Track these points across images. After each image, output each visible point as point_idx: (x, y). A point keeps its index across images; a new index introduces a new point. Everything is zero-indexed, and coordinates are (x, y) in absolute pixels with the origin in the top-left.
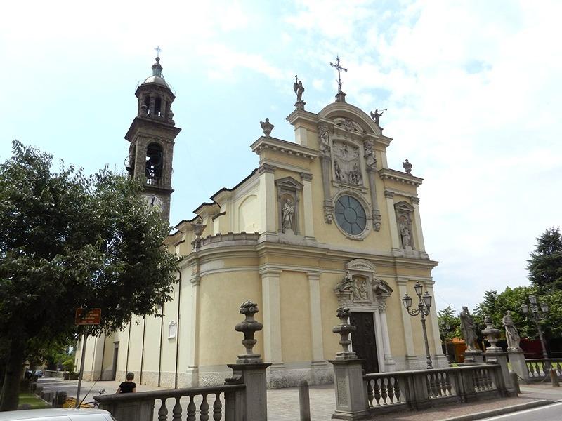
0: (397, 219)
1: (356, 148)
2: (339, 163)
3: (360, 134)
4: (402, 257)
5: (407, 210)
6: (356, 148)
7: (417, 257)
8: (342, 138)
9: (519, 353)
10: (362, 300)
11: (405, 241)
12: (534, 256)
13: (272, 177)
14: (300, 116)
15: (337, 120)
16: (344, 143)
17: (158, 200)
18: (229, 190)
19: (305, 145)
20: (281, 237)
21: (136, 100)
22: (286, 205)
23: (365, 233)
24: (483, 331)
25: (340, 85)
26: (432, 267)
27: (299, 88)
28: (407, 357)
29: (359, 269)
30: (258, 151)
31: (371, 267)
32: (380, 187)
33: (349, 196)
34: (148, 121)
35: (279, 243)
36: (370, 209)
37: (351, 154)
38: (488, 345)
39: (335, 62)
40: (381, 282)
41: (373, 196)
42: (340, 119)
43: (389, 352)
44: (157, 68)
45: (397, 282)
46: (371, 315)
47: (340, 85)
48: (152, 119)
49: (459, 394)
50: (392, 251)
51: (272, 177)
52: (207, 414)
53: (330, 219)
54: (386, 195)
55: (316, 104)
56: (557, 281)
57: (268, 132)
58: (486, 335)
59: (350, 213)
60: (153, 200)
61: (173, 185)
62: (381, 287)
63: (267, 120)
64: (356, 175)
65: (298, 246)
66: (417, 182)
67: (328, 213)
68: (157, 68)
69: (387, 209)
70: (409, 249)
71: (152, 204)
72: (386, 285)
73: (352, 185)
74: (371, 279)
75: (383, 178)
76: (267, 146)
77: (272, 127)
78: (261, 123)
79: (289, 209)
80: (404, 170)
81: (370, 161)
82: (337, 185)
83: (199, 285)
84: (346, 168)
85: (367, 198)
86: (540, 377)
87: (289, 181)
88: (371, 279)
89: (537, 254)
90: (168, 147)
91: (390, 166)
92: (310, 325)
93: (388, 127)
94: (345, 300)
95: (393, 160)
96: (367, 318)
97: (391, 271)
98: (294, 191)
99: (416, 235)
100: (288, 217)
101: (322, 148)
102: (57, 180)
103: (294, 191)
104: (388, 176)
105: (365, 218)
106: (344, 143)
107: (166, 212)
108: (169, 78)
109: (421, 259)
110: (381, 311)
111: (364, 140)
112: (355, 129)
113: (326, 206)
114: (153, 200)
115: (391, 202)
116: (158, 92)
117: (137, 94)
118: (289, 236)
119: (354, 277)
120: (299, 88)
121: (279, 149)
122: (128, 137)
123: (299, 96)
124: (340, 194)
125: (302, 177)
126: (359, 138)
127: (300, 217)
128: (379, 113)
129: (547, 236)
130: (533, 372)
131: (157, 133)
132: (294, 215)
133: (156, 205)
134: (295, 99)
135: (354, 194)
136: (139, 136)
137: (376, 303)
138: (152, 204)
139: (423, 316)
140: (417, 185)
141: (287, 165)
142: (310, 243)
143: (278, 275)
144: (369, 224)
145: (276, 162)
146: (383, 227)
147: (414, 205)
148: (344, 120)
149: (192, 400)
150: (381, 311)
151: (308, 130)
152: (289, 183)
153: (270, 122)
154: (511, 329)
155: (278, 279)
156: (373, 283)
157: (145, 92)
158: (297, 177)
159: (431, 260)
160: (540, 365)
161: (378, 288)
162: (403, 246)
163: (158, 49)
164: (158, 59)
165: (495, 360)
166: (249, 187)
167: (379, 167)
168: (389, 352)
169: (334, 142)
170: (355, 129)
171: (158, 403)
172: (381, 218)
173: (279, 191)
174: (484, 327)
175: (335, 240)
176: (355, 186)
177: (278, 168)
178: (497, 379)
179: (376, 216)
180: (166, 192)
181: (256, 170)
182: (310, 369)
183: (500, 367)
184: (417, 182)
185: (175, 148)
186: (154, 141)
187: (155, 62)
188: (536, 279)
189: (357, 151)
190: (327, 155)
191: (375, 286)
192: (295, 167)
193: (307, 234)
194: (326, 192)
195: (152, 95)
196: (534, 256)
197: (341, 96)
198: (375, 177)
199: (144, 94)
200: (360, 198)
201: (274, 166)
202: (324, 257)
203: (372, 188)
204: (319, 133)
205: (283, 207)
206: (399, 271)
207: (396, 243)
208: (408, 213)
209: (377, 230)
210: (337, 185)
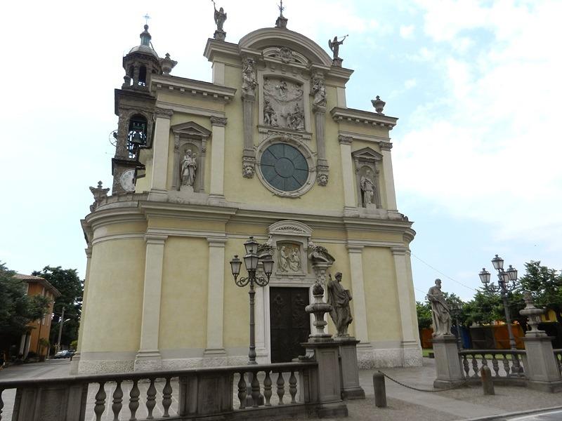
1: (299, 84)
2: (273, 104)
3: (304, 64)
7: (383, 217)
8: (278, 73)
9: (446, 341)
10: (291, 272)
11: (367, 197)
14: (217, 48)
15: (267, 52)
16: (282, 79)
19: (222, 83)
20: (174, 196)
23: (305, 188)
27: (220, 17)
28: (403, 342)
29: (286, 232)
31: (306, 231)
32: (332, 131)
33: (284, 143)
34: (131, 93)
35: (167, 202)
36: (314, 158)
37: (292, 92)
40: (319, 250)
41: (320, 143)
44: (146, 36)
45: (348, 249)
47: (281, 9)
48: (135, 90)
52: (103, 404)
53: (249, 171)
54: (340, 141)
59: (284, 164)
62: (316, 255)
63: (378, 97)
64: (298, 116)
65: (200, 206)
66: (389, 123)
68: (146, 36)
69: (340, 159)
70: (371, 207)
72: (324, 252)
73: (287, 130)
74: (305, 246)
75: (336, 119)
77: (383, 104)
78: (372, 101)
79: (188, 160)
80: (373, 110)
81: (318, 99)
82: (266, 130)
83: (91, 258)
84: (281, 110)
85: (311, 146)
86: (498, 376)
87: (368, 152)
88: (305, 246)
91: (349, 105)
92: (206, 303)
94: (322, 274)
95: (356, 97)
96: (299, 295)
98: (373, 162)
99: (385, 190)
100: (186, 171)
101: (245, 85)
103: (373, 162)
106: (282, 79)
111: (309, 73)
112: (297, 61)
113: (247, 157)
115: (347, 150)
116: (141, 61)
118: (187, 194)
119: (280, 244)
120: (220, 17)
121: (354, 119)
124: (270, 141)
125: (381, 147)
126: (302, 72)
127: (206, 171)
128: (339, 40)
130: (467, 370)
131: (140, 104)
132: (197, 169)
134: (215, 28)
135: (291, 141)
139: (252, 287)
141: (191, 108)
142: (214, 202)
143: (360, 251)
144: (312, 177)
145: (173, 105)
147: (384, 153)
148: (279, 50)
149: (119, 387)
152: (367, 154)
153: (172, 58)
154: (438, 306)
155: (360, 255)
156: (309, 250)
158: (204, 123)
160: (509, 357)
163: (147, 17)
164: (146, 27)
167: (332, 104)
169: (266, 78)
170: (297, 61)
171: (93, 390)
172: (329, 169)
173: (357, 163)
175: (257, 196)
176: (292, 131)
177: (174, 112)
178: (307, 386)
179: (322, 168)
182: (201, 358)
183: (316, 366)
184: (389, 123)
186: (137, 113)
189: (301, 88)
190: (251, 93)
193: (213, 191)
194: (248, 139)
195: (136, 64)
197: (282, 21)
200: (300, 146)
201: (169, 110)
202: (233, 218)
205: (181, 159)
207: (352, 198)
209: (323, 184)
210: (266, 130)
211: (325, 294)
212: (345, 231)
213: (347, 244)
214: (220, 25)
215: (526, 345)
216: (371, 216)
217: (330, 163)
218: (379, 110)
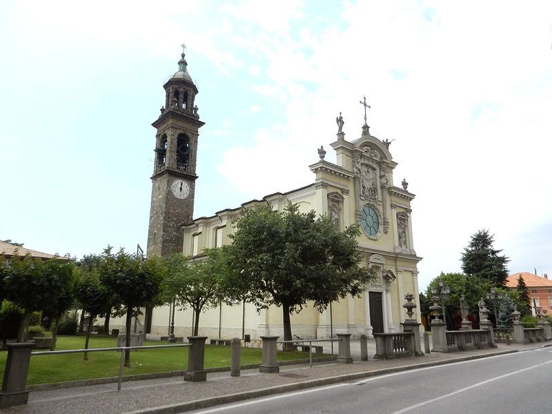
0: (398, 225)
1: (374, 169)
4: (400, 254)
5: (404, 218)
6: (374, 169)
7: (409, 253)
8: (366, 162)
10: (377, 284)
12: (467, 250)
13: (326, 192)
14: (342, 145)
16: (367, 165)
17: (186, 185)
18: (281, 194)
19: (345, 167)
21: (164, 93)
22: (333, 213)
23: (379, 234)
24: (430, 307)
25: (365, 119)
26: (418, 261)
27: (340, 121)
30: (316, 171)
31: (383, 260)
36: (382, 217)
37: (371, 175)
38: (434, 317)
39: (363, 101)
40: (389, 271)
41: (384, 207)
42: (367, 148)
43: (391, 321)
44: (183, 63)
46: (380, 294)
47: (365, 119)
49: (475, 345)
50: (394, 249)
51: (326, 192)
54: (392, 206)
55: (353, 135)
56: (483, 272)
57: (322, 157)
58: (432, 310)
61: (198, 172)
64: (374, 190)
66: (410, 197)
67: (358, 219)
68: (183, 63)
69: (392, 215)
75: (391, 193)
76: (323, 168)
80: (401, 187)
81: (384, 181)
82: (363, 198)
84: (368, 185)
89: (470, 249)
93: (395, 152)
95: (396, 181)
97: (393, 263)
104: (392, 191)
105: (378, 224)
106: (367, 165)
108: (194, 74)
109: (411, 255)
110: (387, 291)
111: (379, 164)
115: (395, 212)
117: (166, 86)
120: (340, 121)
122: (155, 125)
123: (340, 128)
128: (388, 141)
129: (479, 236)
131: (186, 125)
135: (373, 205)
137: (384, 286)
140: (411, 199)
144: (381, 228)
145: (328, 180)
146: (389, 230)
147: (408, 215)
150: (387, 291)
151: (346, 155)
159: (417, 256)
161: (387, 276)
162: (400, 245)
163: (184, 46)
164: (183, 56)
165: (487, 327)
166: (307, 194)
168: (391, 321)
174: (432, 304)
177: (330, 185)
179: (386, 223)
180: (192, 178)
181: (313, 184)
184: (410, 197)
185: (200, 139)
187: (181, 58)
188: (467, 269)
191: (385, 274)
192: (339, 184)
195: (181, 90)
196: (467, 250)
198: (386, 192)
200: (376, 209)
203: (383, 201)
204: (353, 158)
206: (398, 263)
208: (404, 220)
209: (386, 233)
210: (363, 198)
211: (95, 269)
212: (396, 261)
213: (396, 268)
214: (340, 128)
215: (514, 327)
216: (405, 253)
217: (389, 221)
218: (406, 188)
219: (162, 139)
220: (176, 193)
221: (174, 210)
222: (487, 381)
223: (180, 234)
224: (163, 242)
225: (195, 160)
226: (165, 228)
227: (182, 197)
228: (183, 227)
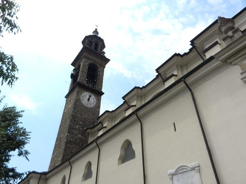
17: (93, 99)
18: (138, 88)
60: (90, 96)
61: (103, 90)
71: (89, 99)
90: (101, 68)
99: (159, 88)
102: (18, 113)
107: (98, 106)
114: (90, 96)
120: (168, 34)
133: (91, 99)
136: (84, 57)
138: (89, 99)
157: (89, 39)
180: (99, 94)
199: (88, 40)
219: (77, 70)
220: (85, 101)
221: (81, 115)
222: (176, 90)
223: (85, 137)
224: (67, 143)
225: (102, 82)
226: (71, 130)
227: (89, 106)
228: (89, 131)
